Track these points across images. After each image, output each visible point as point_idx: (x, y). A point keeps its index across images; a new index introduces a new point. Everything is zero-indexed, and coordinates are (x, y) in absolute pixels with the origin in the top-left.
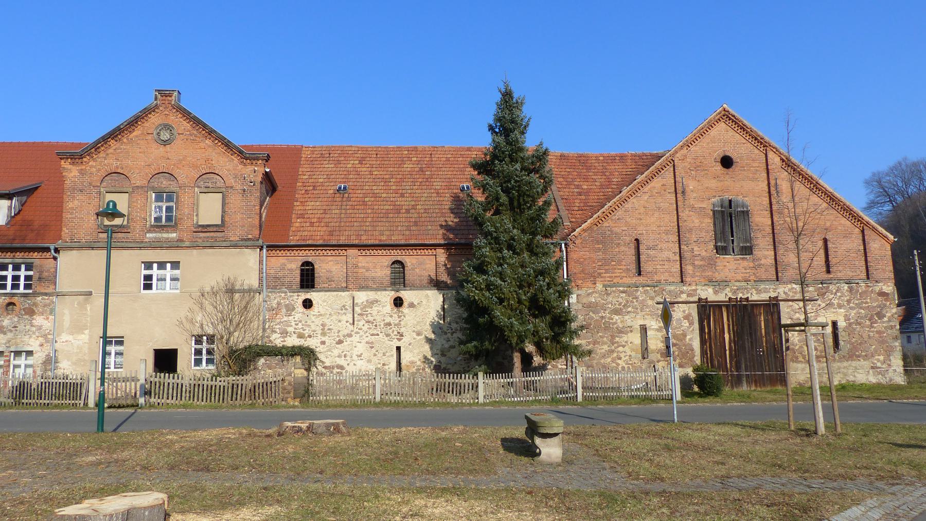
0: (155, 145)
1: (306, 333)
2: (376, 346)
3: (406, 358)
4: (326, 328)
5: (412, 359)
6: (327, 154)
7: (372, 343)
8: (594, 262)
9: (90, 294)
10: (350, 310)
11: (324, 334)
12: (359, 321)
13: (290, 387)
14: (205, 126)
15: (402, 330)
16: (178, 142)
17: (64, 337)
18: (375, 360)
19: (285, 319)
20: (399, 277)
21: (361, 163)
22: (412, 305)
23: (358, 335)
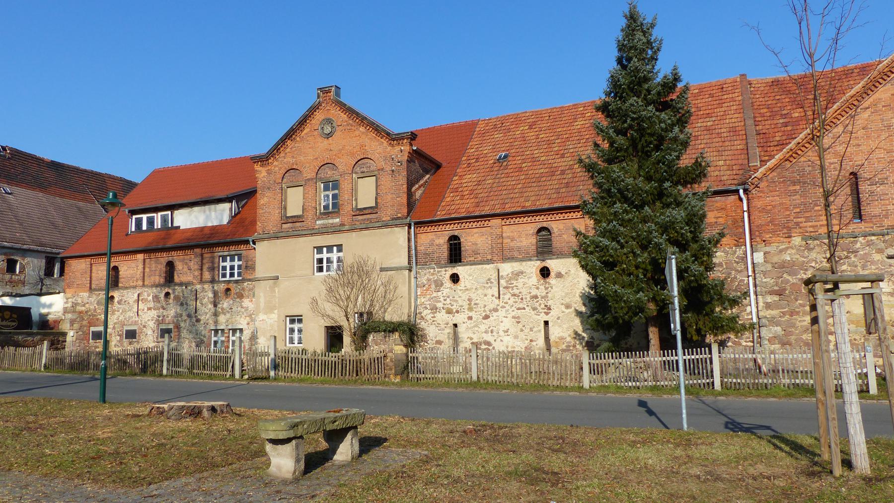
0: (320, 140)
1: (454, 308)
2: (522, 320)
3: (555, 333)
4: (473, 303)
5: (561, 334)
6: (502, 124)
7: (518, 317)
8: (787, 209)
9: (277, 278)
10: (496, 283)
11: (470, 309)
12: (504, 294)
13: (391, 364)
14: (357, 114)
15: (550, 303)
16: (338, 134)
17: (262, 316)
18: (522, 335)
19: (435, 294)
20: (545, 246)
21: (530, 127)
22: (559, 275)
23: (504, 310)
